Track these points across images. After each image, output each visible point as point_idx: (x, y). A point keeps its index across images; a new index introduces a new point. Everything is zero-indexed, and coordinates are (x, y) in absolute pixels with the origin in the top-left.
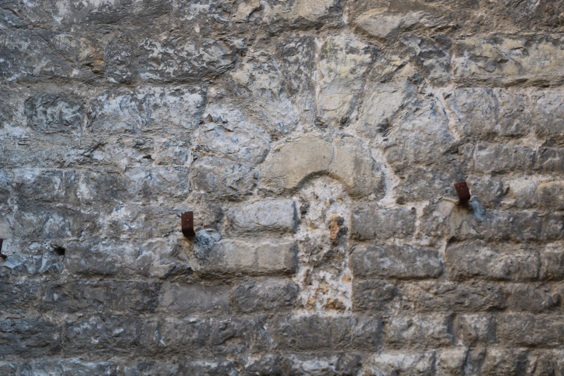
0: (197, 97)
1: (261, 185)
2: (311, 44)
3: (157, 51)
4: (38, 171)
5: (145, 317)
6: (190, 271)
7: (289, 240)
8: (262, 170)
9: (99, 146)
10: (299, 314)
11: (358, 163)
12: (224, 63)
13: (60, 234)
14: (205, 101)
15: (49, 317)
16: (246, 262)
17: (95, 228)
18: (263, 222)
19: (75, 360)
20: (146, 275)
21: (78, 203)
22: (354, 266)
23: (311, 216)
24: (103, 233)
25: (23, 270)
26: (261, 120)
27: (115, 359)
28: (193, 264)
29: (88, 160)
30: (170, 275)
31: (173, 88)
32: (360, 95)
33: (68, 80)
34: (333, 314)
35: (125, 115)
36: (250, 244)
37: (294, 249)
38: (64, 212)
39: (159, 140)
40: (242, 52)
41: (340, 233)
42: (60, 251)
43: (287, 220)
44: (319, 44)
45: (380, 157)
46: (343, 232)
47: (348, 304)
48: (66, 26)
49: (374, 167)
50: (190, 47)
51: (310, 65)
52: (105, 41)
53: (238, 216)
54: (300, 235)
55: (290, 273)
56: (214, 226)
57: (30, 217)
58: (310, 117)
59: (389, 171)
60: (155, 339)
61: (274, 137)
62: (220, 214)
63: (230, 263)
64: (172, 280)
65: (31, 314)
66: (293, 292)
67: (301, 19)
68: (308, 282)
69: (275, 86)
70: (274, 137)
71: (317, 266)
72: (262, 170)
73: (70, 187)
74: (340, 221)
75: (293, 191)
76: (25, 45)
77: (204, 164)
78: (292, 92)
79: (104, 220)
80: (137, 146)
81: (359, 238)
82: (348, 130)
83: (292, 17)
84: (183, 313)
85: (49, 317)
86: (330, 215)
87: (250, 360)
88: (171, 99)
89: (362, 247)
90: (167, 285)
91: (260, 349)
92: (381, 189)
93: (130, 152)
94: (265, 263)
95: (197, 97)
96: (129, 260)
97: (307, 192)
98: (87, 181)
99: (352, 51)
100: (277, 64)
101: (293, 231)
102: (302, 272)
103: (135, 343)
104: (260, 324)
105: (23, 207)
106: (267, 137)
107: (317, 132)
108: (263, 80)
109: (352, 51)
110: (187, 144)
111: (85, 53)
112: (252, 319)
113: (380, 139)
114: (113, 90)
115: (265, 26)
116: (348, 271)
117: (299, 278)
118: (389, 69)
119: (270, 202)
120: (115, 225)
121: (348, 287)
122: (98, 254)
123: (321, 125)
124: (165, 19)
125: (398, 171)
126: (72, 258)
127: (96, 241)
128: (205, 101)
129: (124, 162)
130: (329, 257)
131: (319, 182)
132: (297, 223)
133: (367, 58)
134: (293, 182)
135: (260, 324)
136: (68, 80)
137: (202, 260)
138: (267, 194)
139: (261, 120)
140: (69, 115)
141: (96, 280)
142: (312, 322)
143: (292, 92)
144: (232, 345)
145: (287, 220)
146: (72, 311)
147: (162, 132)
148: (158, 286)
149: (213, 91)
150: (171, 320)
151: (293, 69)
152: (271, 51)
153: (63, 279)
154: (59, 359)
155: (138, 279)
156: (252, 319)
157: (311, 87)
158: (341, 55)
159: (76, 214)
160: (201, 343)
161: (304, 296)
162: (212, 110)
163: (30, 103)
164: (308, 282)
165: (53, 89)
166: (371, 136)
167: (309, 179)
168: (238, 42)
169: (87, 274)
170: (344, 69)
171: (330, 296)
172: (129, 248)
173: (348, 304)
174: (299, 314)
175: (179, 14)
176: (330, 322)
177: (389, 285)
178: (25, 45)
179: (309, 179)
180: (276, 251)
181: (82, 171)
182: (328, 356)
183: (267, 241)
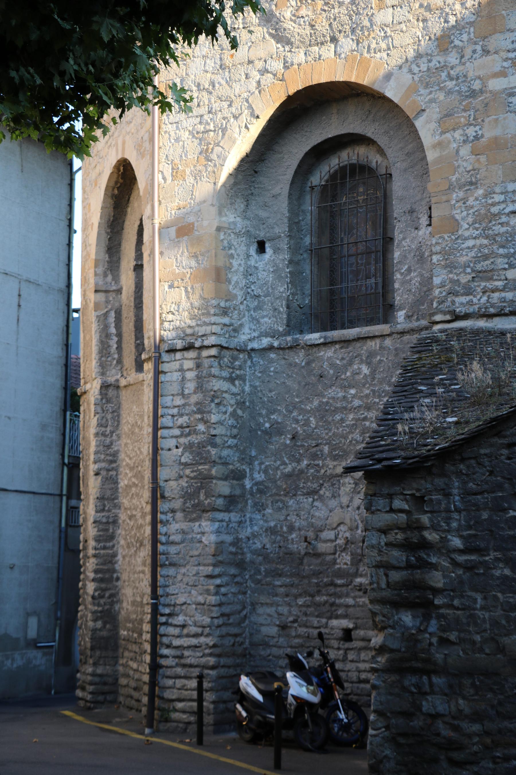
0: (311, 500)
1: (328, 527)
2: (340, 482)
3: (302, 485)
4: (274, 523)
5: (300, 566)
6: (310, 553)
7: (334, 544)
8: (328, 522)
9: (288, 515)
10: (337, 566)
11: (351, 519)
12: (318, 488)
13: (280, 542)
14: (314, 500)
15: (278, 566)
16: (323, 550)
17: (288, 540)
18: (328, 538)
19: (284, 579)
20: (300, 554)
21: (284, 532)
22: (351, 552)
23: (340, 536)
24: (290, 541)
25: (271, 552)
26: (327, 506)
27: (294, 579)
28: (311, 551)
29: (286, 519)
30: (306, 554)
31: (306, 496)
32: (352, 498)
33: (280, 495)
34: (345, 566)
35: (294, 505)
36: (324, 545)
37: (335, 546)
38: (281, 535)
39: (303, 513)
40: (322, 485)
41: (139, 263)
42: (280, 547)
43: (333, 537)
44: (342, 481)
45: (357, 517)
46: (348, 541)
47: (349, 563)
48: (280, 478)
49: (356, 521)
50: (309, 484)
51: (339, 489)
52: (289, 482)
53: (322, 536)
54: (337, 542)
55: (334, 554)
56: (316, 539)
57: (273, 537)
58: (339, 505)
59: (359, 522)
60: (479, 412)
61: (331, 511)
62: (317, 536)
63: (319, 551)
64: (121, 656)
65: (274, 565)
66: (335, 560)
67: (336, 474)
68: (339, 557)
69: (330, 495)
70: (331, 511)
71: (342, 551)
72: (328, 522)
73: (281, 528)
74: (347, 538)
75: (335, 529)
76: (270, 485)
77: (313, 521)
78: (335, 497)
79: (290, 538)
80: (297, 515)
81: (352, 543)
82: (349, 509)
83: (334, 473)
84: (309, 566)
85: (278, 566)
86: (344, 536)
87: (325, 580)
88: (305, 500)
89: (353, 546)
90: (305, 557)
91: (328, 577)
92: (357, 528)
93: (295, 517)
94: (328, 551)
95: (311, 500)
96: (296, 550)
97: (339, 528)
98: (286, 526)
99: (350, 484)
100: (331, 488)
101: (335, 541)
102: (338, 554)
103: (298, 574)
104: (327, 569)
105: (271, 534)
106: (328, 512)
107: (341, 510)
108: (328, 494)
109: (350, 484)
110: (309, 514)
111: (284, 487)
112: (325, 568)
113: (357, 512)
114: (291, 498)
115: (328, 476)
116: (349, 553)
117: (337, 556)
118: (359, 489)
119: (330, 532)
120: (292, 539)
121: (349, 558)
122: (289, 548)
123: (342, 507)
124: (303, 475)
125: (362, 522)
126: (283, 549)
127: (288, 544)
128: (314, 500)
129: (294, 520)
130: (344, 549)
131: (342, 526)
132: (336, 538)
133: (353, 486)
134: (335, 525)
135: (327, 569)
136: (280, 495)
137: (313, 550)
138: (328, 529)
139: (327, 506)
140: (281, 505)
141: (288, 556)
142: (339, 569)
143: (335, 497)
144: (321, 575)
145: (333, 537)
146: (283, 565)
147: (303, 510)
148: (303, 558)
149: (316, 497)
150: (306, 568)
151: (335, 490)
152: (330, 484)
153: (281, 555)
154: (281, 578)
155: (298, 556)
156: (325, 568)
157: (339, 495)
158: (347, 485)
159: (283, 536)
160: (313, 574)
161: (338, 561)
162: (316, 504)
163: (272, 502)
164: (339, 557)
165: (277, 498)
166: (355, 511)
167: (339, 525)
168: (321, 482)
169: (286, 554)
170: (348, 490)
171: (344, 561)
172: (296, 546)
173: (349, 563)
174: (337, 566)
175: (307, 473)
176: (344, 569)
177: (359, 558)
178: (270, 485)
179: (339, 525)
180: (331, 547)
181: (284, 523)
182: (344, 579)
183: (329, 544)
